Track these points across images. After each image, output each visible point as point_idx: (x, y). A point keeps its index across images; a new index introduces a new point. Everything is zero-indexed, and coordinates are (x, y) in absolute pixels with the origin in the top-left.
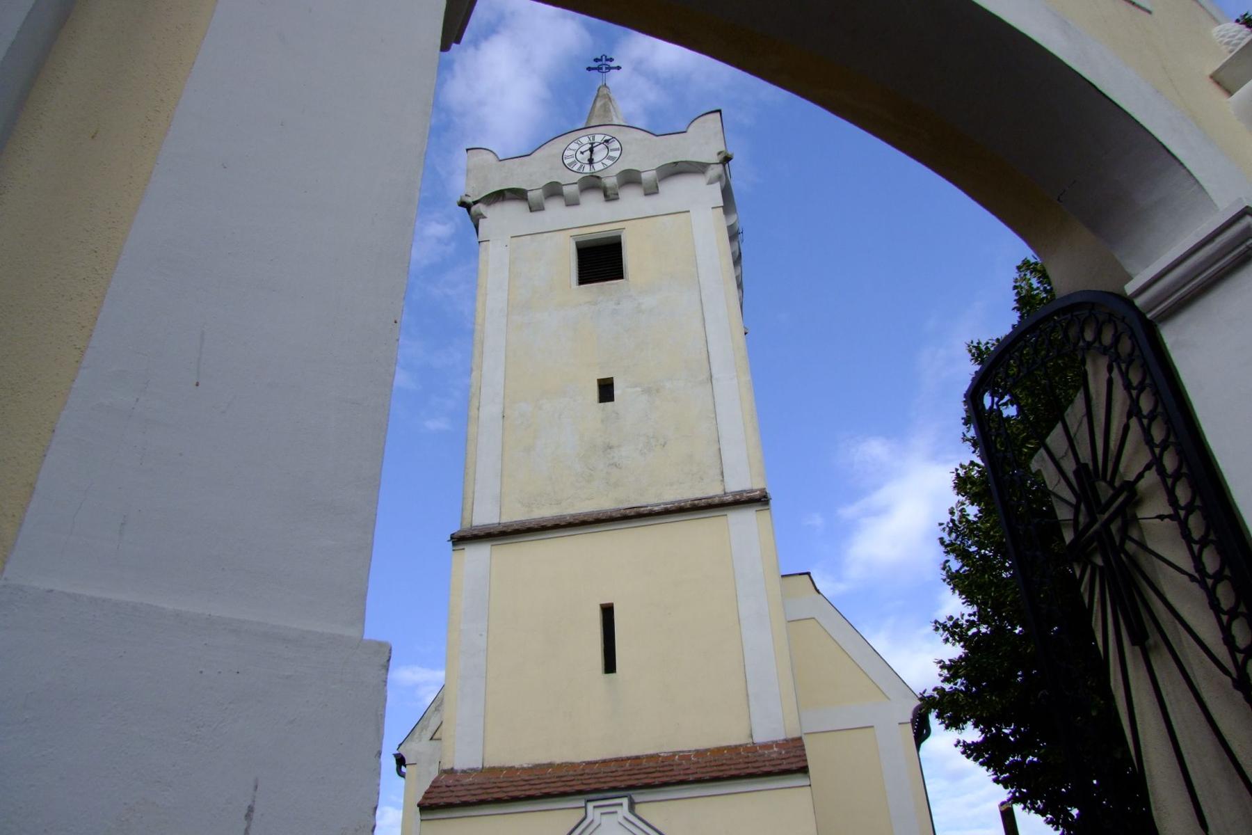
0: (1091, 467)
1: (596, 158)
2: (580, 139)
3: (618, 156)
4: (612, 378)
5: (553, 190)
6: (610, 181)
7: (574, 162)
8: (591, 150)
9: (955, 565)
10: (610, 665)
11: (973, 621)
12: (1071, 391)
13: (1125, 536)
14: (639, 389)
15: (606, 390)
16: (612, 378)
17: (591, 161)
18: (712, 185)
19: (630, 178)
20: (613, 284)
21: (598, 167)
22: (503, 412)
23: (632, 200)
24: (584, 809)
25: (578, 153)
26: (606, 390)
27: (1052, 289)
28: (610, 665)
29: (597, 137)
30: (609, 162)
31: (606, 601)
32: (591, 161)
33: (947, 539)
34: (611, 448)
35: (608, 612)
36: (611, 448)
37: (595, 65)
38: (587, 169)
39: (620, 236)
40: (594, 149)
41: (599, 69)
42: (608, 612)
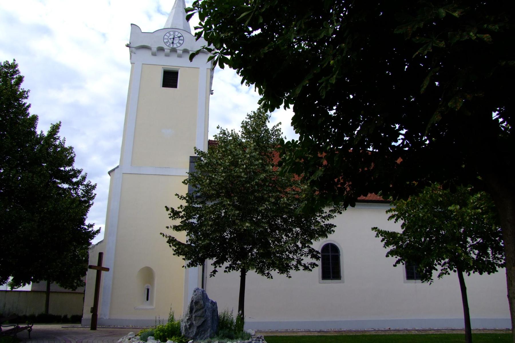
1: (175, 42)
2: (170, 32)
3: (182, 43)
4: (176, 86)
5: (161, 49)
8: (174, 39)
9: (183, 237)
11: (217, 50)
12: (191, 178)
16: (176, 86)
17: (173, 43)
18: (198, 41)
21: (175, 46)
24: (45, 296)
25: (169, 39)
27: (195, 151)
29: (176, 32)
30: (179, 45)
32: (173, 43)
33: (183, 237)
38: (171, 46)
39: (178, 71)
40: (175, 39)
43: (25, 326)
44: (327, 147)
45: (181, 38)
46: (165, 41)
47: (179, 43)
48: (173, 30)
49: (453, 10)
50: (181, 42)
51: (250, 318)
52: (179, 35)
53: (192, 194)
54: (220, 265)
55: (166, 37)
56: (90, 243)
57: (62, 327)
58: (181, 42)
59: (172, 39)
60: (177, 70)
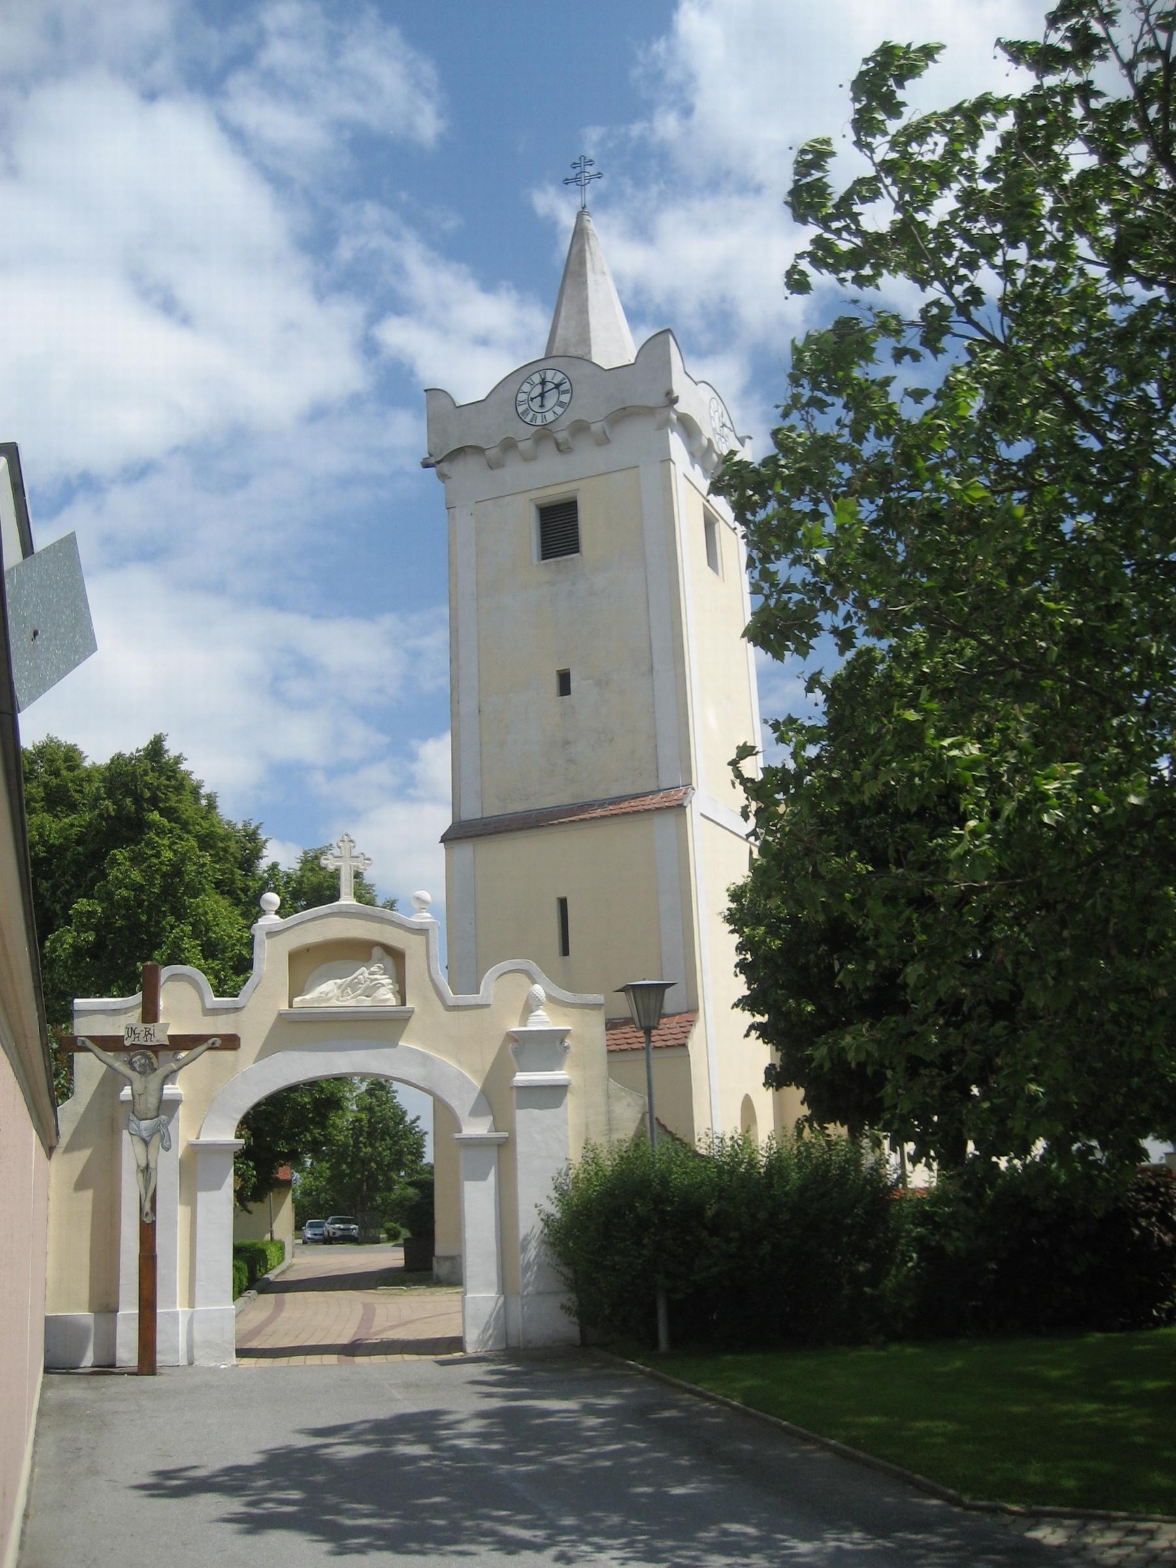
0: (1134, 567)
5: (509, 445)
6: (562, 436)
7: (527, 410)
10: (565, 951)
13: (322, 1091)
14: (591, 681)
15: (564, 683)
19: (580, 428)
20: (568, 560)
22: (479, 706)
23: (587, 457)
24: (643, 1055)
26: (564, 683)
28: (565, 951)
30: (559, 410)
31: (562, 895)
34: (568, 743)
35: (563, 903)
36: (568, 743)
37: (572, 174)
39: (576, 497)
41: (576, 180)
42: (563, 903)
43: (507, 1528)
44: (412, 1541)
45: (562, 388)
46: (521, 409)
47: (561, 404)
48: (534, 368)
49: (736, 1146)
50: (565, 398)
51: (36, 633)
52: (559, 378)
53: (1013, 1031)
54: (308, 1199)
55: (522, 397)
56: (770, 1166)
57: (712, 559)
58: (565, 398)
59: (539, 398)
60: (571, 495)
